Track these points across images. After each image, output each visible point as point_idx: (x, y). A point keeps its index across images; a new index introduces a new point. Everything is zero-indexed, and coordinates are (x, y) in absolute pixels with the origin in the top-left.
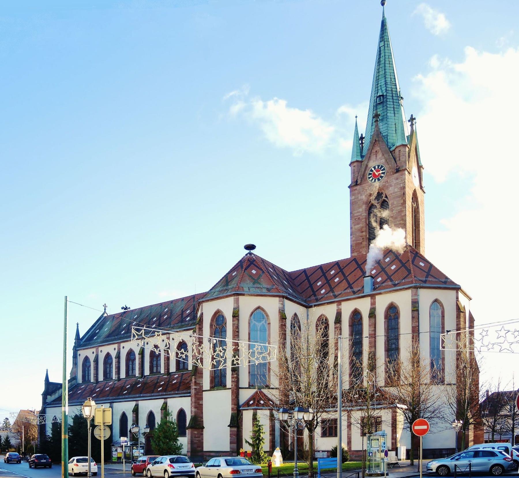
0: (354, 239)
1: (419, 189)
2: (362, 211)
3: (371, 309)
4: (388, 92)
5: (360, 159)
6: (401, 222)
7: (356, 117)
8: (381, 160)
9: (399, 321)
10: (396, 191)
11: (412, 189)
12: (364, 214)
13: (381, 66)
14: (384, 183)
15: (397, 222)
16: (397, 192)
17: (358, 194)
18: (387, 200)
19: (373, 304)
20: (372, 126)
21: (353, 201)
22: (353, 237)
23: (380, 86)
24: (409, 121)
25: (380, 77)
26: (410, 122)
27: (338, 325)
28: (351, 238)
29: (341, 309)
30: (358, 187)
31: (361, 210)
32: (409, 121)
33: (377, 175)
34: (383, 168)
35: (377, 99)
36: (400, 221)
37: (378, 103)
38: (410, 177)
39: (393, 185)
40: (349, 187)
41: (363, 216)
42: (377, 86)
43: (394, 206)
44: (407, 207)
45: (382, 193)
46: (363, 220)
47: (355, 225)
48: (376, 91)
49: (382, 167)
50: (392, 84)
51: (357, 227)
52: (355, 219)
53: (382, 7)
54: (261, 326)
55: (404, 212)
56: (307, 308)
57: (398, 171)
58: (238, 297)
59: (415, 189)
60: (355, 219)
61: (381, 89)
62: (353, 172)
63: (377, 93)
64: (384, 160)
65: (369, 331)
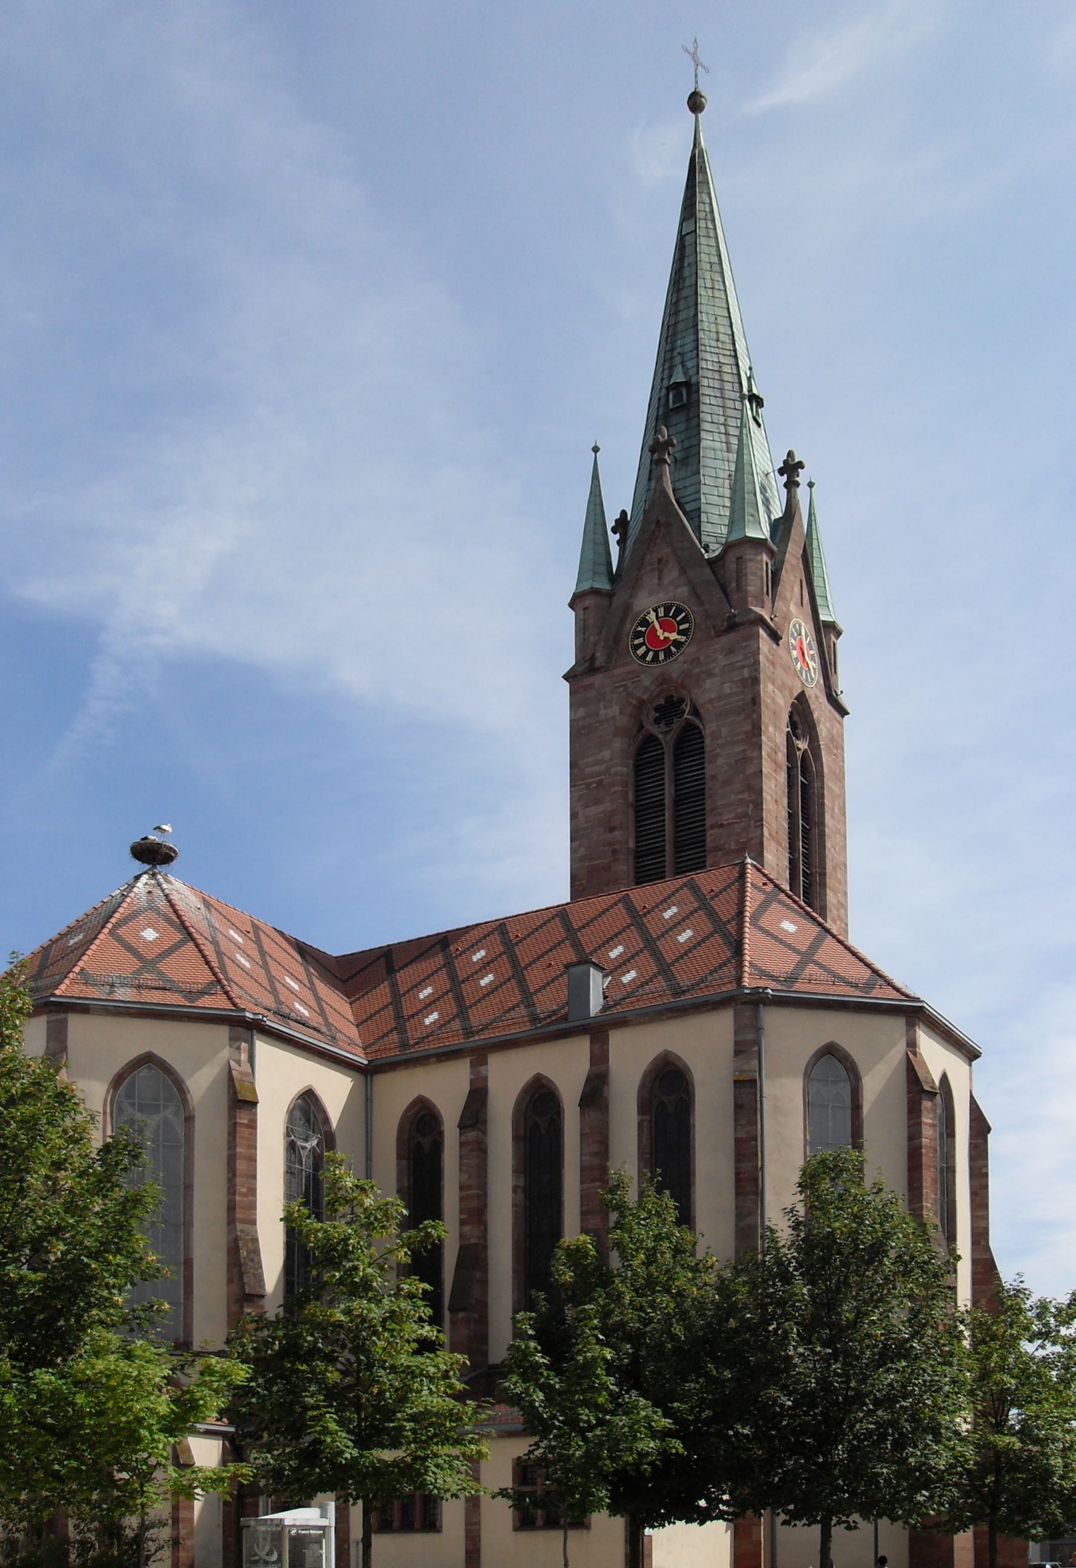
0: (582, 851)
1: (823, 699)
2: (611, 759)
3: (589, 1080)
4: (717, 385)
5: (606, 586)
6: (745, 796)
7: (596, 450)
8: (677, 587)
9: (691, 1121)
10: (729, 691)
11: (791, 693)
12: (619, 769)
13: (685, 293)
14: (686, 666)
15: (733, 795)
16: (730, 695)
17: (599, 701)
18: (697, 721)
19: (600, 1058)
20: (650, 479)
21: (581, 723)
22: (580, 846)
23: (679, 354)
24: (781, 472)
25: (680, 326)
26: (785, 476)
27: (472, 1135)
28: (573, 851)
29: (486, 1079)
30: (597, 679)
31: (606, 754)
32: (781, 472)
33: (662, 638)
34: (684, 614)
35: (667, 395)
36: (743, 792)
37: (671, 406)
38: (781, 651)
39: (717, 670)
40: (566, 677)
41: (616, 774)
42: (668, 355)
43: (720, 742)
44: (764, 747)
45: (682, 701)
46: (613, 790)
47: (587, 806)
48: (666, 372)
49: (679, 611)
50: (722, 352)
51: (593, 810)
52: (588, 786)
53: (693, 116)
54: (158, 1127)
55: (755, 761)
56: (366, 1076)
57: (732, 626)
58: (62, 1016)
59: (802, 694)
60: (588, 786)
61: (683, 363)
62: (582, 630)
63: (670, 376)
64: (683, 591)
65: (581, 1155)
